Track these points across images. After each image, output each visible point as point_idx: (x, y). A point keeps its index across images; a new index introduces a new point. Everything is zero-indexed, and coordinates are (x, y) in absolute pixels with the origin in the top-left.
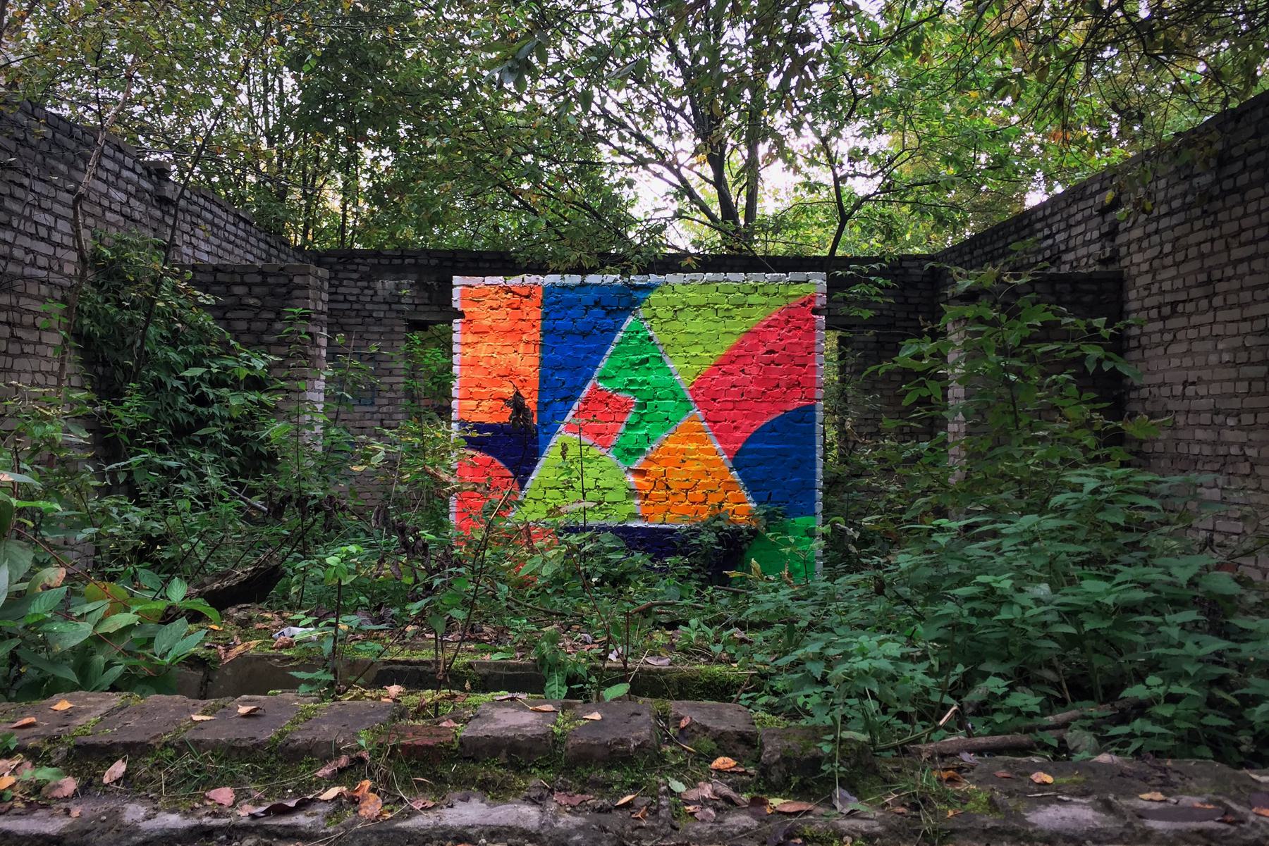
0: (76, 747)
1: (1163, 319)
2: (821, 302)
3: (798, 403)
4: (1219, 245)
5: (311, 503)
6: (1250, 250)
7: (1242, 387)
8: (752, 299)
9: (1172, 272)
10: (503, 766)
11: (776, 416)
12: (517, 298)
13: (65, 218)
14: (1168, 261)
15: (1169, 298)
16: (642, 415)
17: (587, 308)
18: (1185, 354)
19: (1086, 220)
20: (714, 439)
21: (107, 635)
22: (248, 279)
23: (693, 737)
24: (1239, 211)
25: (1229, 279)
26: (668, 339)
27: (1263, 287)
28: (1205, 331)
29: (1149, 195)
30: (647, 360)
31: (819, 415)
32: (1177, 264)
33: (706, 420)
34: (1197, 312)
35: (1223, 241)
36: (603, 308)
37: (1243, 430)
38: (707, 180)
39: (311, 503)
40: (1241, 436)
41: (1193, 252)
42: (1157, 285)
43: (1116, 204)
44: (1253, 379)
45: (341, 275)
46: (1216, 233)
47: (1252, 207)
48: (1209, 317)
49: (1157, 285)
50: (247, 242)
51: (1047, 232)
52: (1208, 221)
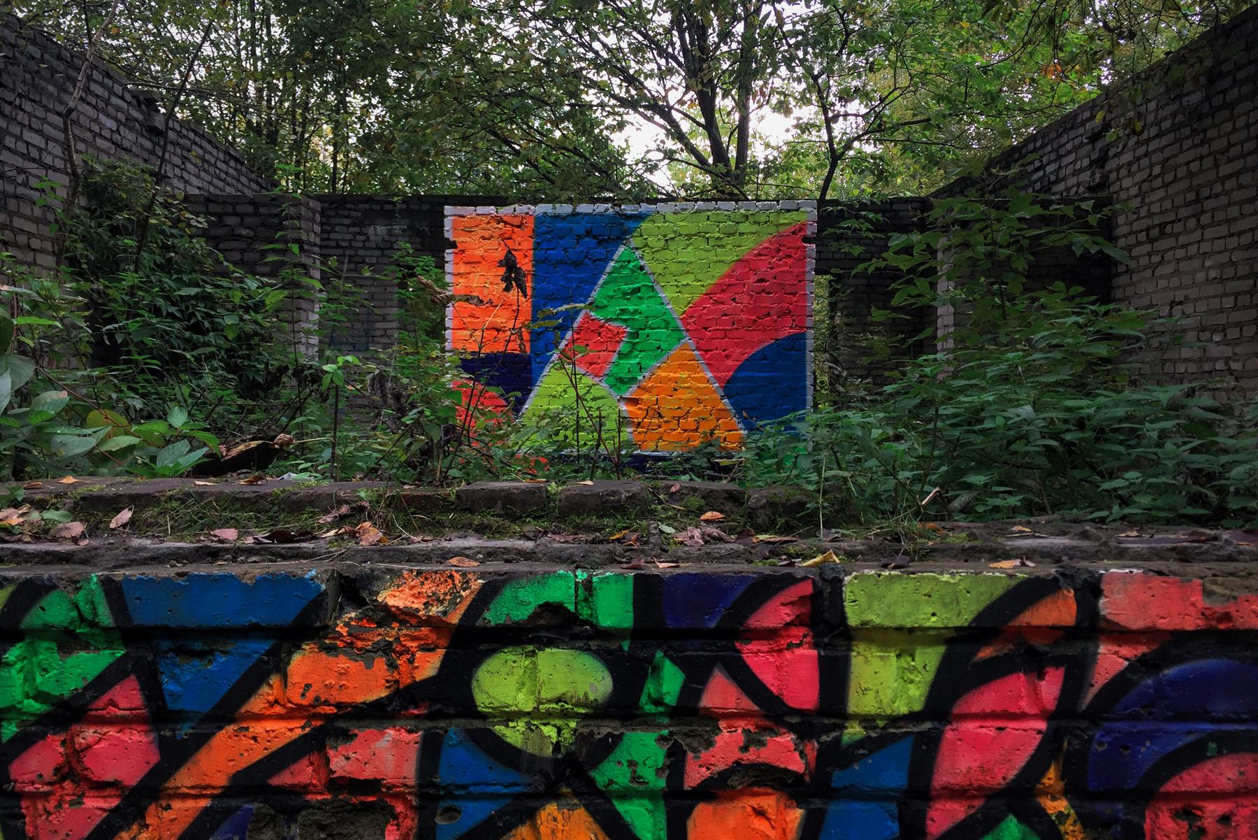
0: (83, 499)
1: (1151, 241)
2: (811, 230)
3: (787, 332)
4: (1208, 162)
5: (307, 372)
6: (1238, 165)
7: (1228, 303)
8: (744, 227)
9: (1161, 193)
10: (498, 515)
11: (766, 344)
12: (509, 228)
13: (55, 141)
14: (1158, 182)
15: (1157, 220)
16: (634, 344)
17: (579, 237)
18: (1172, 275)
19: (1076, 149)
20: (705, 367)
21: (111, 452)
22: (240, 209)
23: (682, 499)
24: (1228, 127)
25: (1217, 196)
26: (659, 268)
27: (1251, 201)
28: (1192, 250)
29: (1139, 115)
30: (638, 290)
31: (810, 344)
32: (1165, 186)
33: (698, 349)
34: (1186, 231)
35: (1211, 158)
36: (595, 237)
37: (1228, 345)
38: (699, 124)
39: (307, 372)
40: (1228, 351)
41: (1182, 172)
42: (1146, 208)
43: (1106, 126)
44: (1239, 293)
45: (333, 221)
46: (1205, 150)
47: (1241, 122)
48: (1197, 236)
49: (1146, 208)
50: (238, 180)
51: (1037, 164)
52: (1197, 140)
